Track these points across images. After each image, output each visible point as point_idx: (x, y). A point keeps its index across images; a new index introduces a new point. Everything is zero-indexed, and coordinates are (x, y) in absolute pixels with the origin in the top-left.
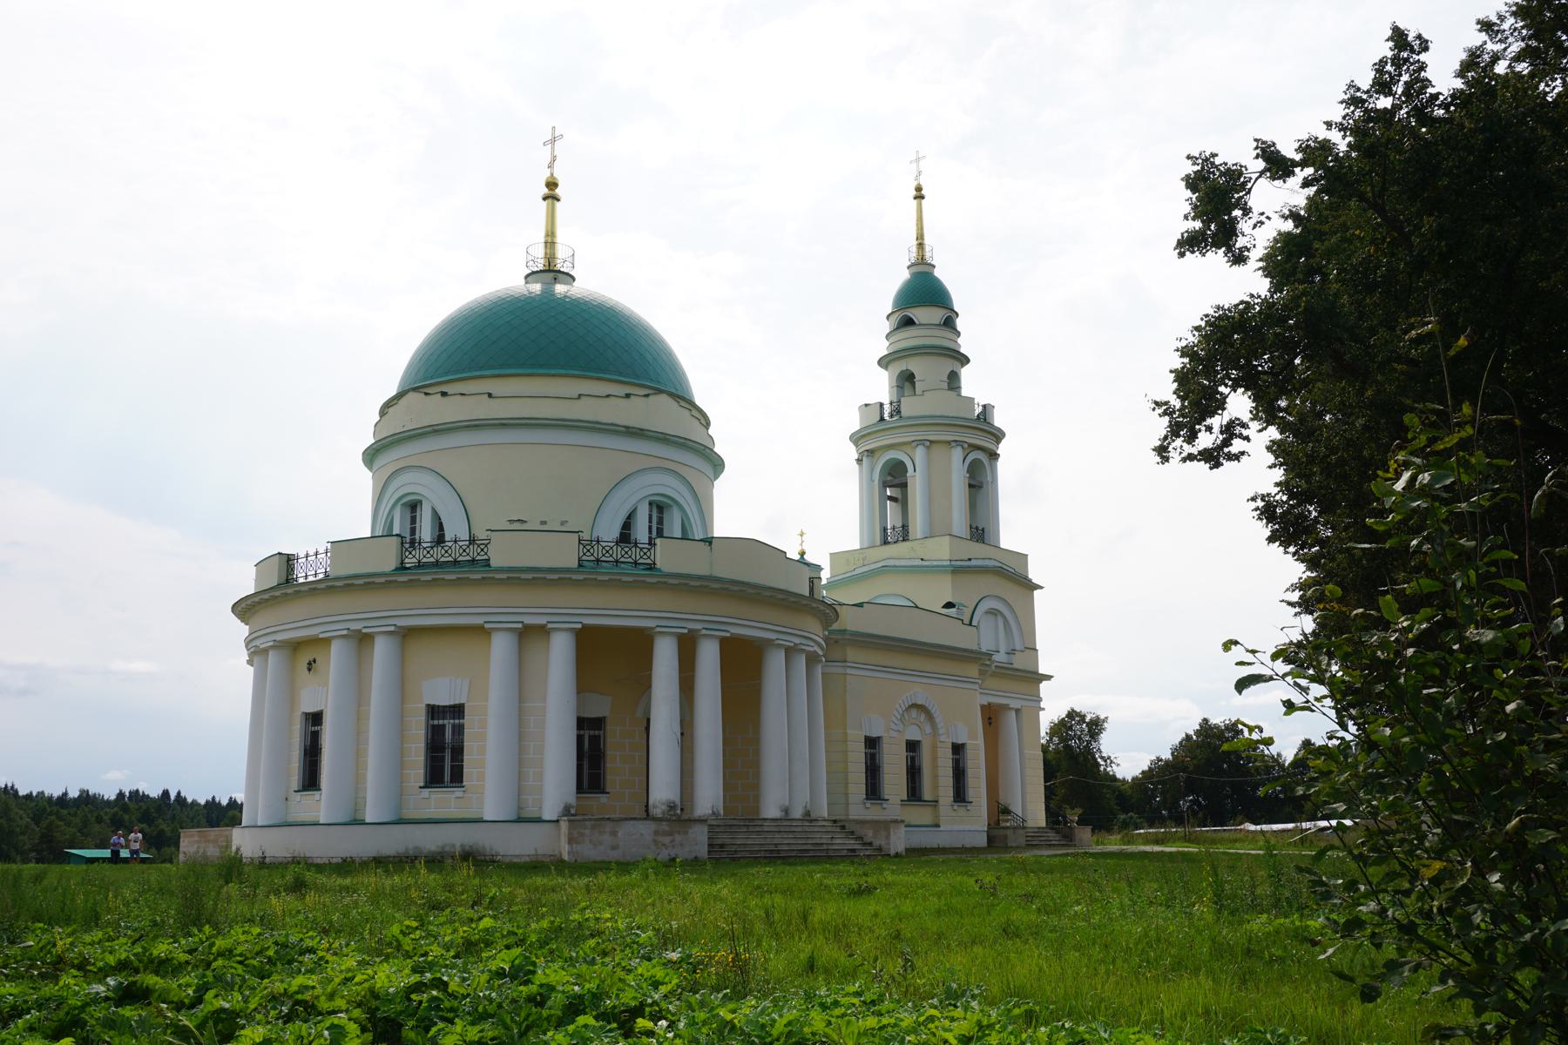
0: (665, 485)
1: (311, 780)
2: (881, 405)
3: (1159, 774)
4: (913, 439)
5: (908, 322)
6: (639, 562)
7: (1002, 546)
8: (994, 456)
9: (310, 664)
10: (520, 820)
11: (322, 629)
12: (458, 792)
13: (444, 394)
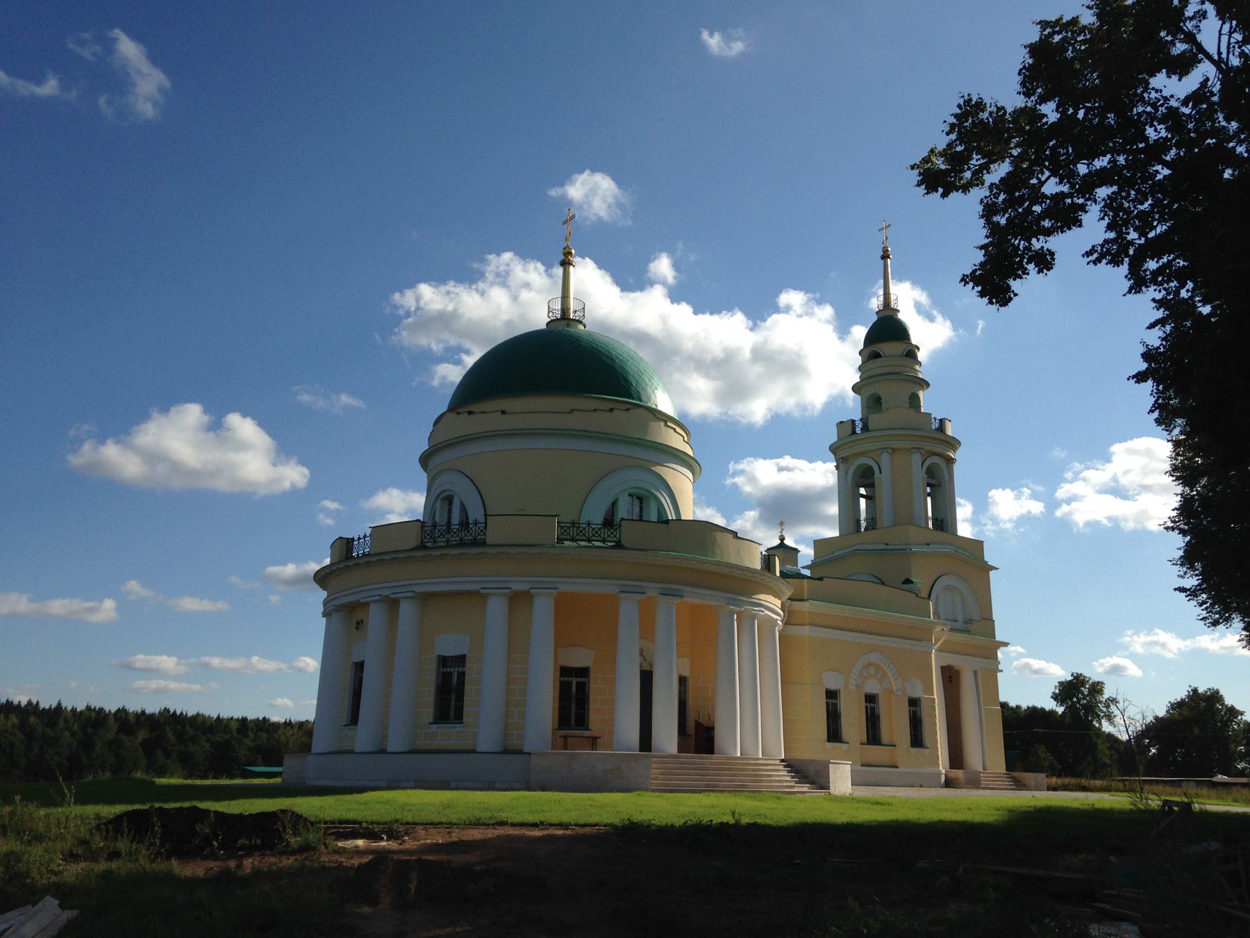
0: (635, 479)
1: (354, 719)
2: (853, 422)
3: (1158, 730)
4: (877, 447)
5: (874, 356)
6: (607, 539)
7: (959, 534)
8: (951, 461)
9: (358, 623)
10: (506, 751)
11: (365, 594)
12: (458, 727)
13: (470, 413)
